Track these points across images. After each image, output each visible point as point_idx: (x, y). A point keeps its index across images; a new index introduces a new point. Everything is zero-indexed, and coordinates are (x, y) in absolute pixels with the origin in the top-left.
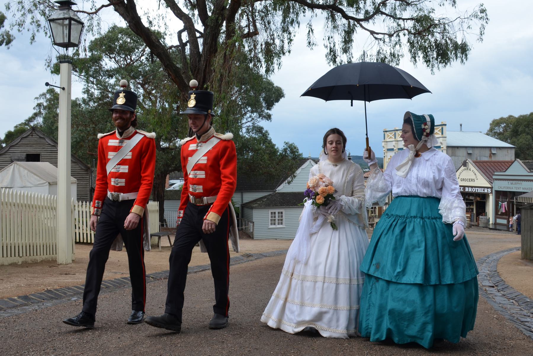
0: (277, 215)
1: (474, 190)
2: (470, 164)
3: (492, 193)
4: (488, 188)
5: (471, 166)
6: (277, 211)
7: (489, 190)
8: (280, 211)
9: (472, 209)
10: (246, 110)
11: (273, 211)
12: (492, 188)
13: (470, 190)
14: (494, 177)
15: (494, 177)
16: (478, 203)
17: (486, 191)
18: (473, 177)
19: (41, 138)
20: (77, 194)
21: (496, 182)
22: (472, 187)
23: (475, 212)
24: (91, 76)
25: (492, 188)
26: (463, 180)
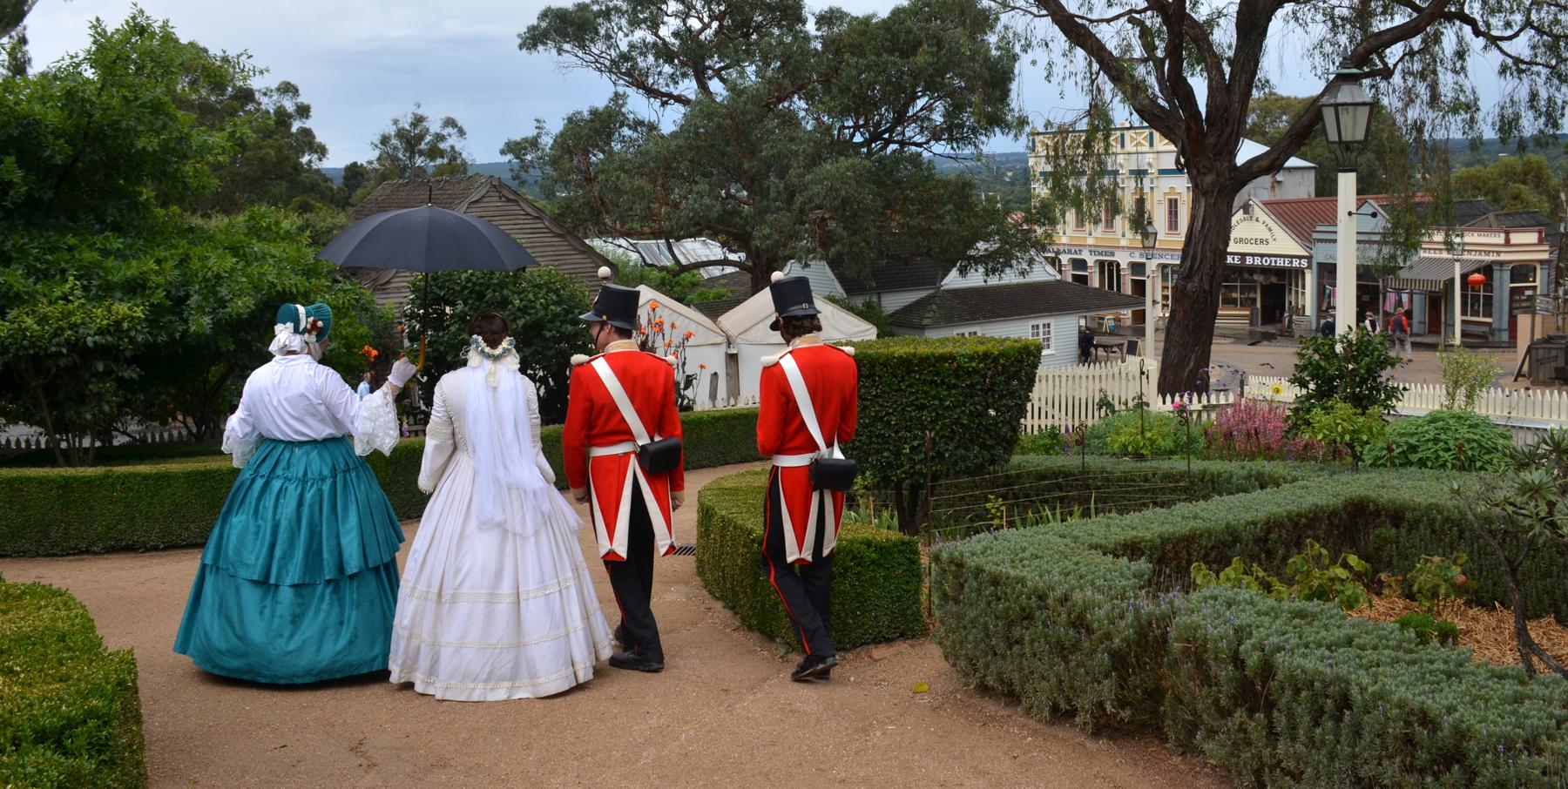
0: (1041, 330)
1: (1266, 262)
2: (1256, 209)
3: (1309, 267)
4: (1300, 257)
5: (1258, 212)
6: (1041, 322)
7: (1304, 263)
8: (1046, 321)
9: (1254, 300)
10: (1040, 148)
11: (1035, 322)
12: (1309, 258)
13: (1258, 261)
14: (1315, 236)
15: (1315, 236)
16: (1266, 290)
17: (1296, 263)
18: (1266, 235)
19: (509, 200)
20: (1359, 287)
21: (1319, 245)
22: (1262, 256)
23: (1259, 305)
24: (776, 92)
25: (1309, 258)
26: (1241, 240)
